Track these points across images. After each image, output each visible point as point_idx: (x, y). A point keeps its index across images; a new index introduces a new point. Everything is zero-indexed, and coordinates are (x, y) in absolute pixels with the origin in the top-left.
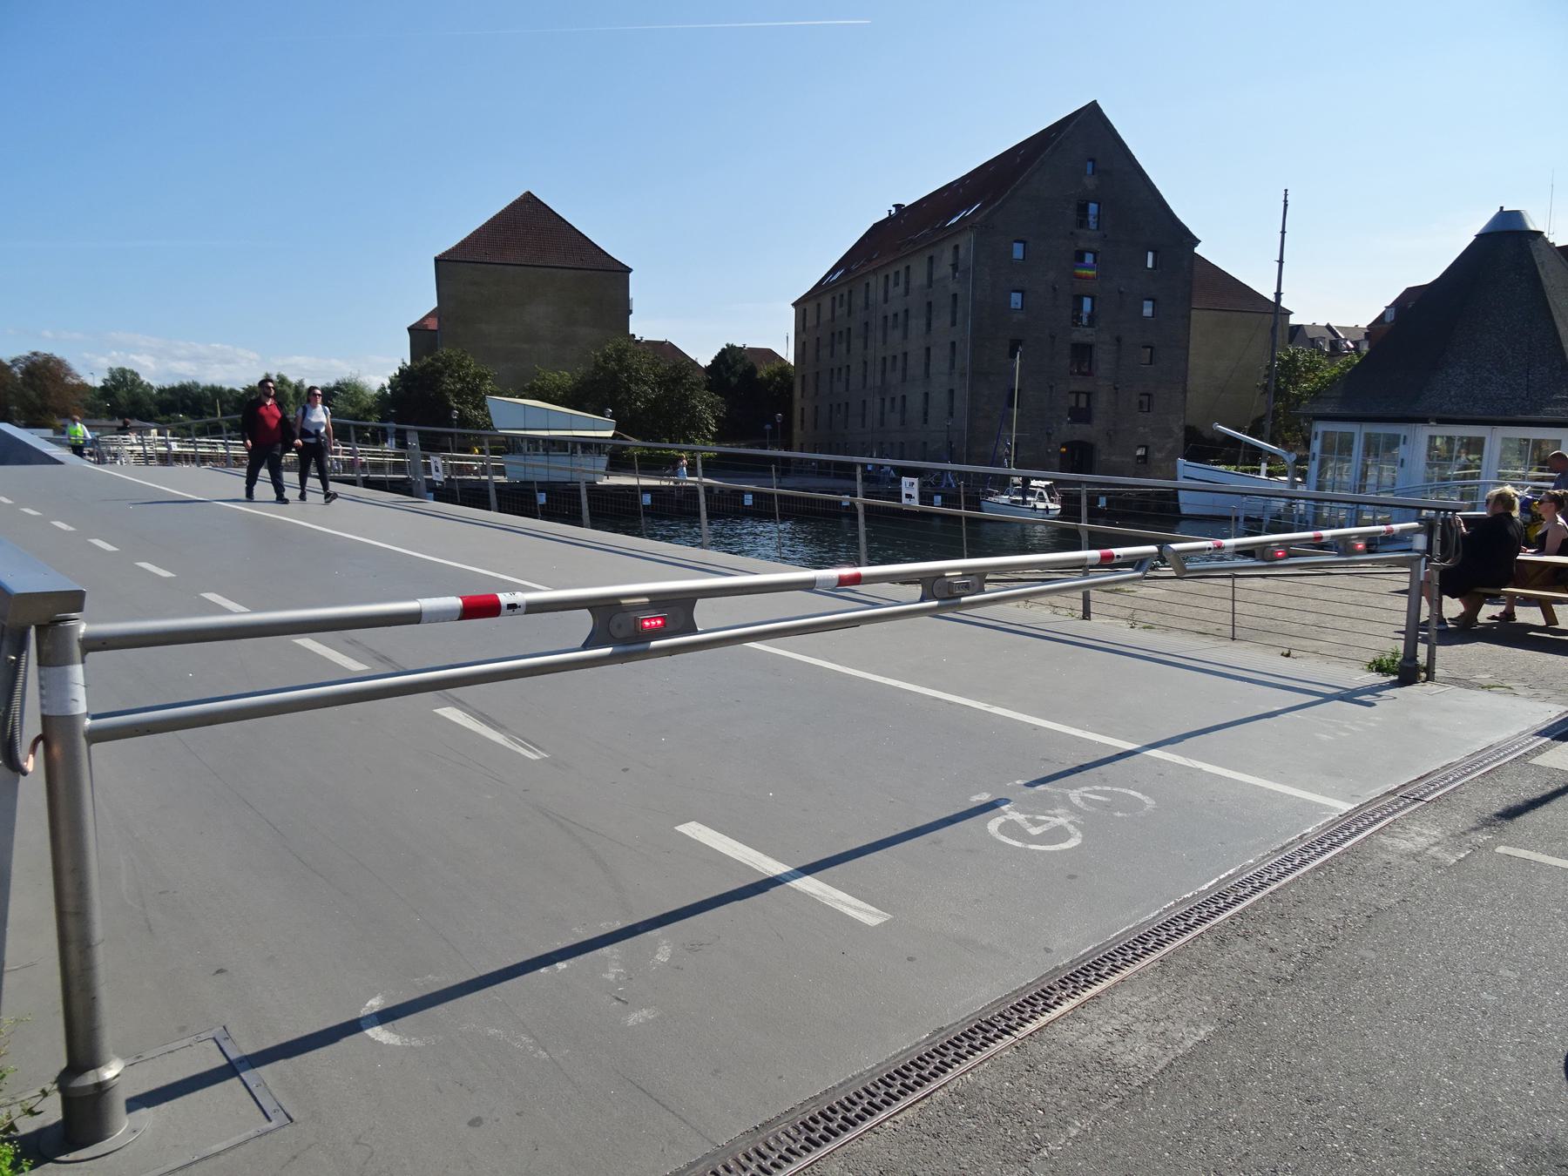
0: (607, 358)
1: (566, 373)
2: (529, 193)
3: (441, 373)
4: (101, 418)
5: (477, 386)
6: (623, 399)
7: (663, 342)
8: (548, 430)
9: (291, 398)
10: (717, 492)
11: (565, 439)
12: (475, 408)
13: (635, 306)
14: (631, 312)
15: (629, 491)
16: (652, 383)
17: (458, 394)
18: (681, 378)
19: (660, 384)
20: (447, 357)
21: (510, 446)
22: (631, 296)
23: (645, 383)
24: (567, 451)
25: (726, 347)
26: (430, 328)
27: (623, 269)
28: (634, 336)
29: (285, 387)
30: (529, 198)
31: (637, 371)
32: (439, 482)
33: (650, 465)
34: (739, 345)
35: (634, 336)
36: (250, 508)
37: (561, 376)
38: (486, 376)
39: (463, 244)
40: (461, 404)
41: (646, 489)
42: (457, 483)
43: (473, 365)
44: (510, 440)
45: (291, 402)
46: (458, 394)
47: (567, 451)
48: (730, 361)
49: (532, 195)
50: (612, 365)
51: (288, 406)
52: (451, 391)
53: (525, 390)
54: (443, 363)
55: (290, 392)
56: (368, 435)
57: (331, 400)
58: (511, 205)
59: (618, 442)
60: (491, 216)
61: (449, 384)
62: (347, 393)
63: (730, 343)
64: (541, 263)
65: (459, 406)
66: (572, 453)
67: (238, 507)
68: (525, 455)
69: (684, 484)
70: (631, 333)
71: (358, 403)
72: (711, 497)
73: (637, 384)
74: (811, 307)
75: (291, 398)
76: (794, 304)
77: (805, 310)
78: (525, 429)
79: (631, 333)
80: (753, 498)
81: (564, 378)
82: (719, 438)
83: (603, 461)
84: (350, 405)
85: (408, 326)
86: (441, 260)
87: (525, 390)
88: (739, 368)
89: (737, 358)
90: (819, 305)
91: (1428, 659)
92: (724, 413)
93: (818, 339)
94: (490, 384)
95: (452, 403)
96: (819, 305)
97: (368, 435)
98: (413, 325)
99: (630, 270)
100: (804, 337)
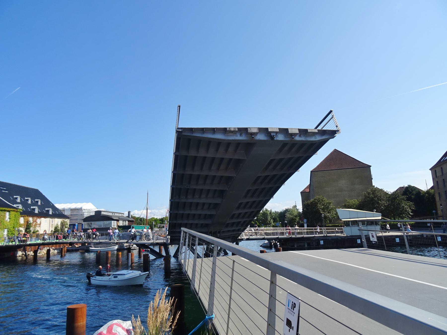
0: (369, 194)
1: (356, 200)
2: (335, 149)
3: (317, 204)
4: (262, 226)
5: (328, 206)
6: (377, 206)
7: (403, 187)
8: (358, 218)
9: (269, 214)
10: (425, 236)
11: (373, 220)
12: (328, 213)
13: (373, 177)
14: (372, 179)
15: (390, 237)
16: (386, 200)
17: (323, 209)
18: (397, 198)
19: (388, 200)
20: (318, 199)
21: (347, 224)
22: (372, 174)
23: (383, 200)
24: (365, 225)
25: (408, 186)
26: (307, 192)
27: (368, 166)
28: (374, 186)
29: (267, 212)
30: (336, 151)
31: (380, 197)
32: (374, 241)
33: (394, 227)
34: (412, 185)
35: (374, 186)
36: (298, 252)
37: (355, 201)
38: (330, 203)
39: (318, 166)
40: (324, 212)
41: (397, 236)
42: (291, 235)
43: (326, 200)
44: (345, 222)
45: (269, 216)
46: (323, 209)
47: (365, 225)
48: (410, 191)
49: (336, 150)
50: (371, 196)
51: (268, 217)
52: (320, 208)
53: (343, 206)
54: (317, 200)
55: (269, 213)
56: (296, 223)
57: (286, 214)
58: (331, 153)
59: (383, 220)
60: (49, 200)
61: (320, 206)
62: (290, 212)
63: (409, 185)
64: (342, 168)
65: (323, 213)
66: (367, 225)
67: (296, 252)
68: (351, 227)
69: (412, 234)
70: (373, 185)
71: (293, 214)
72: (423, 238)
73: (380, 201)
74: (438, 170)
75: (269, 214)
76: (431, 169)
77: (435, 171)
78: (350, 218)
79: (373, 185)
80: (441, 238)
81: (356, 201)
82: (413, 217)
83: (378, 228)
84: (291, 215)
85: (301, 192)
86: (312, 172)
87: (343, 206)
88: (414, 192)
89: (413, 189)
90: (442, 168)
91: (116, 221)
92: (414, 208)
93: (444, 180)
94: (332, 205)
95: (321, 212)
96: (442, 168)
97: (296, 223)
98: (302, 191)
99: (371, 166)
100: (437, 180)
